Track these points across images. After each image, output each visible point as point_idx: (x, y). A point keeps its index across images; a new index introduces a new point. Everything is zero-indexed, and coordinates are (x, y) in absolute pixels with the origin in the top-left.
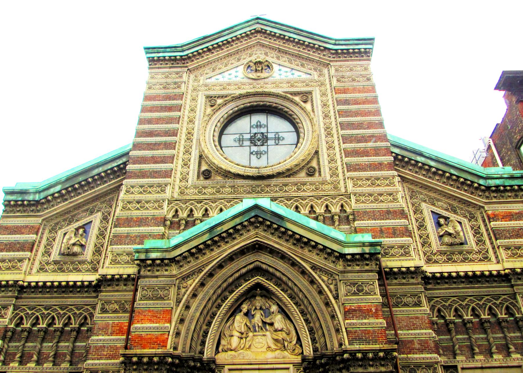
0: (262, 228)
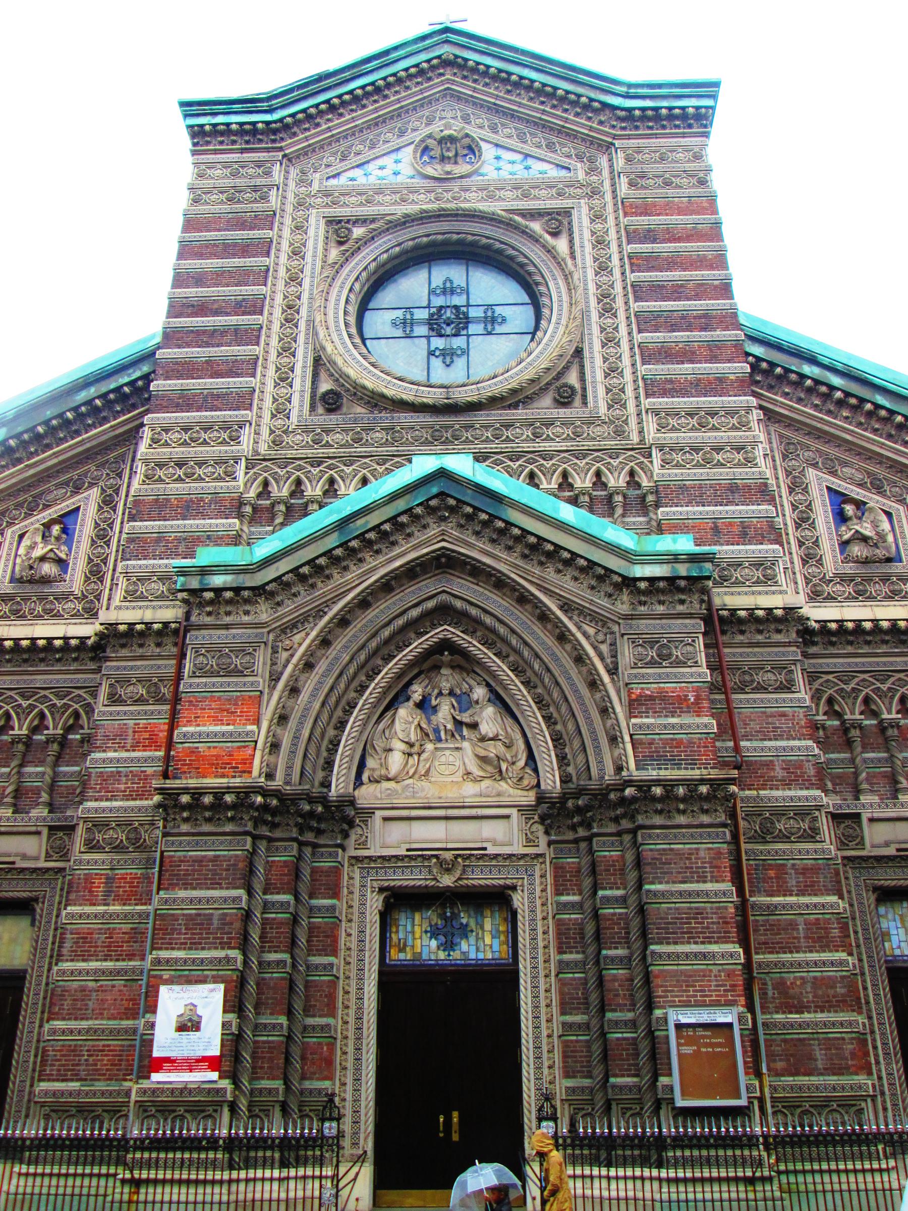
0: (454, 520)
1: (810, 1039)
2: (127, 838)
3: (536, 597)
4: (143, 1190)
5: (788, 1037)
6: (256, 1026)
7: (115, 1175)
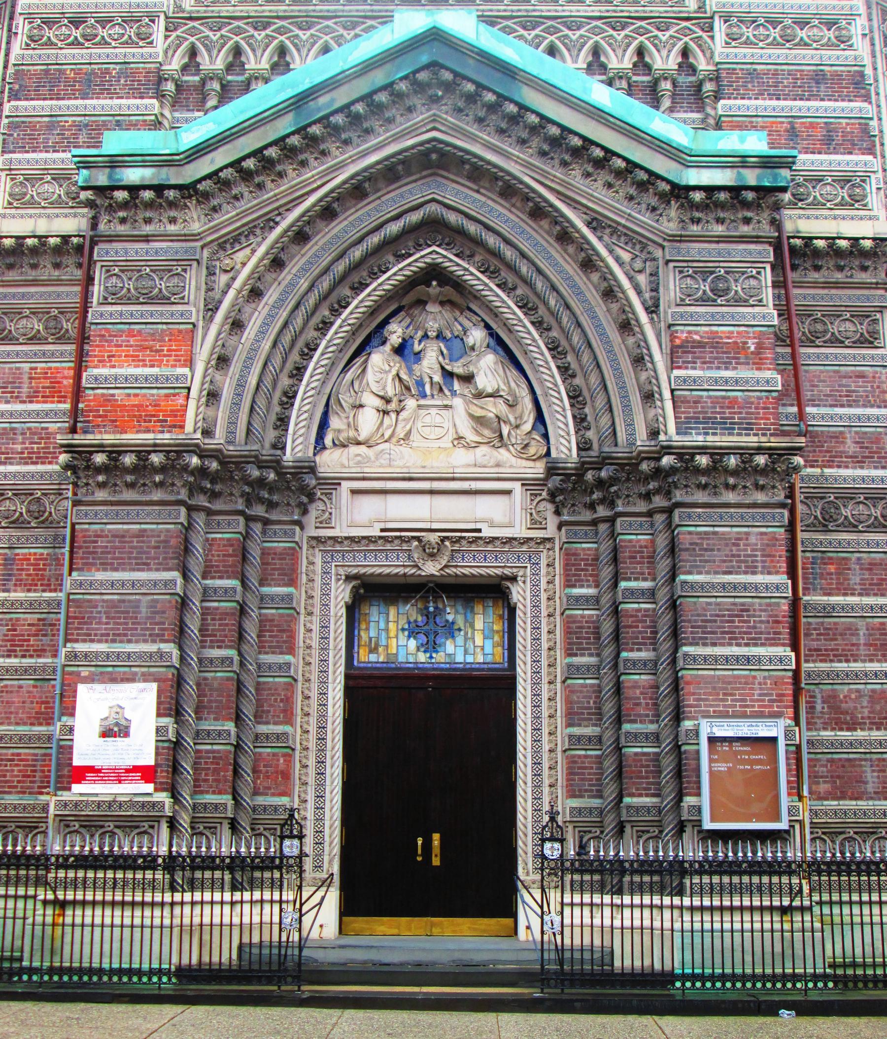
0: (449, 102)
1: (861, 760)
2: (28, 511)
3: (557, 210)
4: (69, 912)
5: (836, 756)
6: (198, 733)
7: (35, 897)
